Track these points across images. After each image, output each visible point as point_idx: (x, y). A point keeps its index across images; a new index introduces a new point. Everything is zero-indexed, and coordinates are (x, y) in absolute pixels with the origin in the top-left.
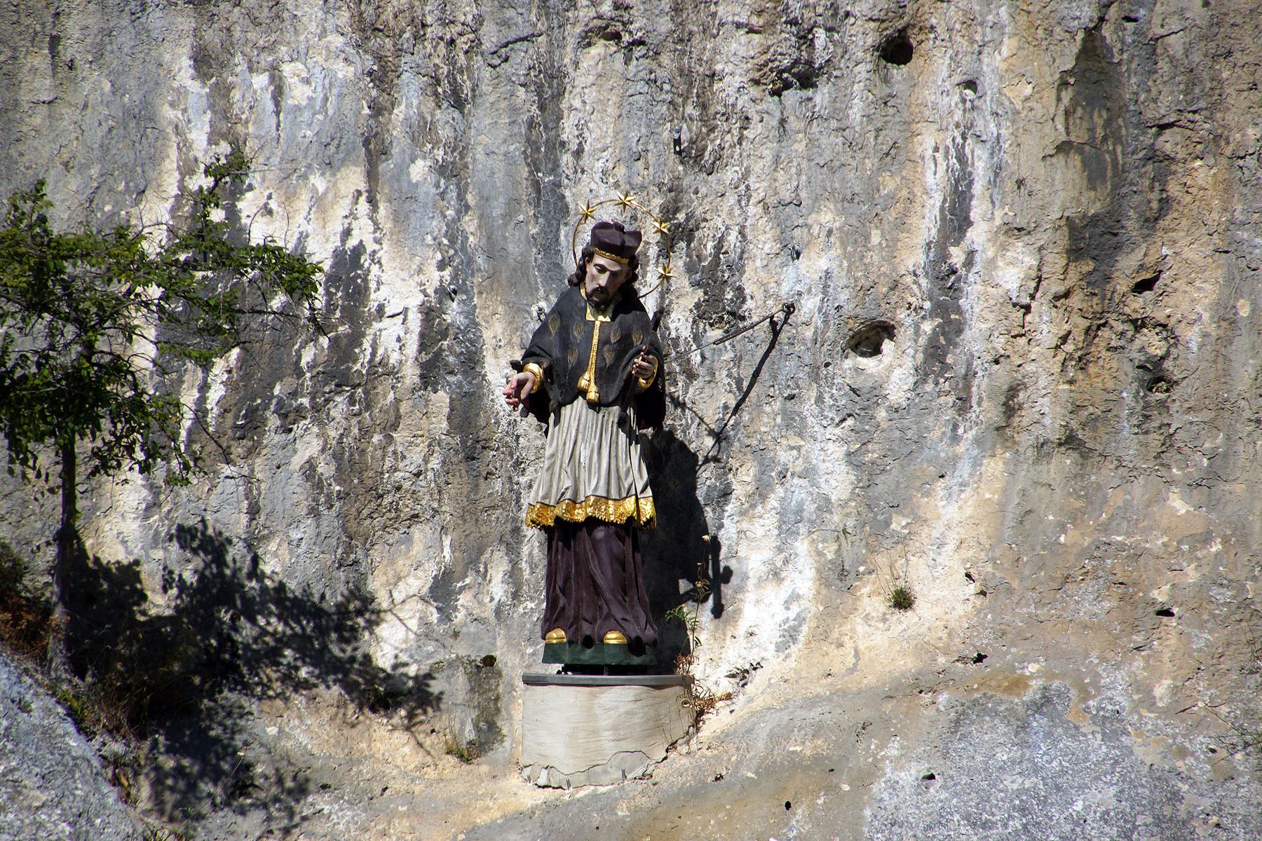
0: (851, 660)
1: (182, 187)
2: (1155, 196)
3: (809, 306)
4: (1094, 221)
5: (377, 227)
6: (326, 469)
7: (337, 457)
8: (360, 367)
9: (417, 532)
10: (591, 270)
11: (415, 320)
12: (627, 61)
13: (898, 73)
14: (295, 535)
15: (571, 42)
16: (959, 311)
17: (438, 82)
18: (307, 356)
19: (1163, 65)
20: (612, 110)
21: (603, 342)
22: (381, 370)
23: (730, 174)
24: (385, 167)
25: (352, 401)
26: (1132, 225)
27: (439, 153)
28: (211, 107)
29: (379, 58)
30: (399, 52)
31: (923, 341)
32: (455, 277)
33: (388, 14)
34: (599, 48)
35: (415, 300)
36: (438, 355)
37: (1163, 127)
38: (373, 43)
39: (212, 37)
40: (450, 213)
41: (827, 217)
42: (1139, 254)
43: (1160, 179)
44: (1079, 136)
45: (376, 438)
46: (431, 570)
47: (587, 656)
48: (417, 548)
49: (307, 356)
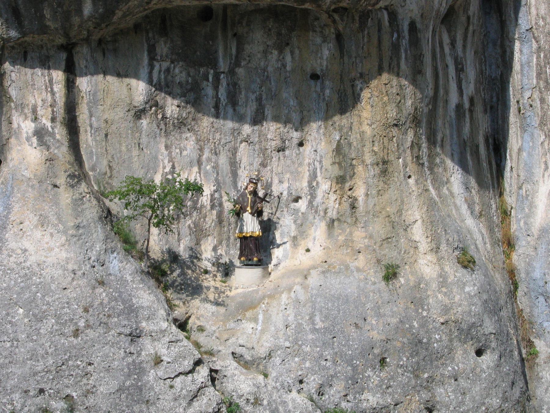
0: (299, 262)
1: (163, 171)
2: (352, 172)
3: (285, 193)
4: (341, 177)
5: (201, 179)
6: (192, 226)
7: (194, 224)
8: (199, 205)
9: (209, 238)
10: (249, 187)
11: (209, 197)
12: (249, 146)
13: (301, 149)
14: (187, 239)
15: (238, 143)
16: (315, 194)
17: (212, 150)
18: (189, 204)
19: (353, 148)
20: (246, 155)
21: (251, 201)
22: (202, 206)
23: (269, 168)
24: (203, 167)
25: (197, 212)
26: (348, 178)
27: (212, 164)
28: (168, 156)
29: (201, 146)
30: (204, 145)
31: (308, 200)
32: (217, 189)
33: (202, 138)
34: (244, 144)
35: (209, 193)
36: (214, 203)
37: (353, 159)
38: (200, 143)
39: (169, 143)
40: (215, 176)
41: (288, 175)
42: (350, 183)
43: (353, 169)
44: (337, 161)
45: (202, 220)
46: (212, 245)
47: (250, 263)
48: (209, 241)
49: (189, 204)
